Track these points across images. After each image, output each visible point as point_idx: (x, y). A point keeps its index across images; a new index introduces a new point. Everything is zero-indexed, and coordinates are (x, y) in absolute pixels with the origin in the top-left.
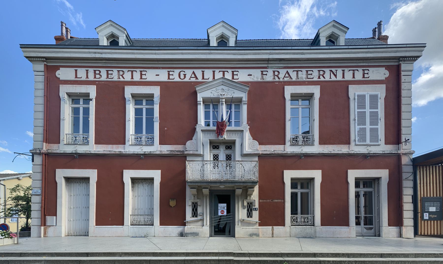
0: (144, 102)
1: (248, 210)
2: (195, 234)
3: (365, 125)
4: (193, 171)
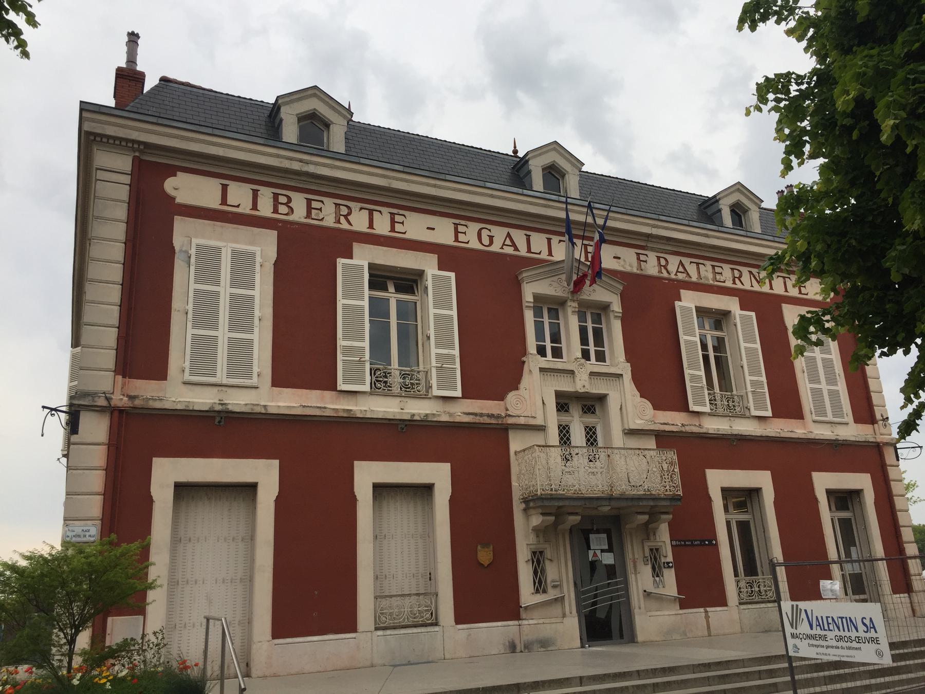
0: (391, 289)
1: (654, 568)
2: (545, 643)
3: (216, 328)
4: (540, 466)
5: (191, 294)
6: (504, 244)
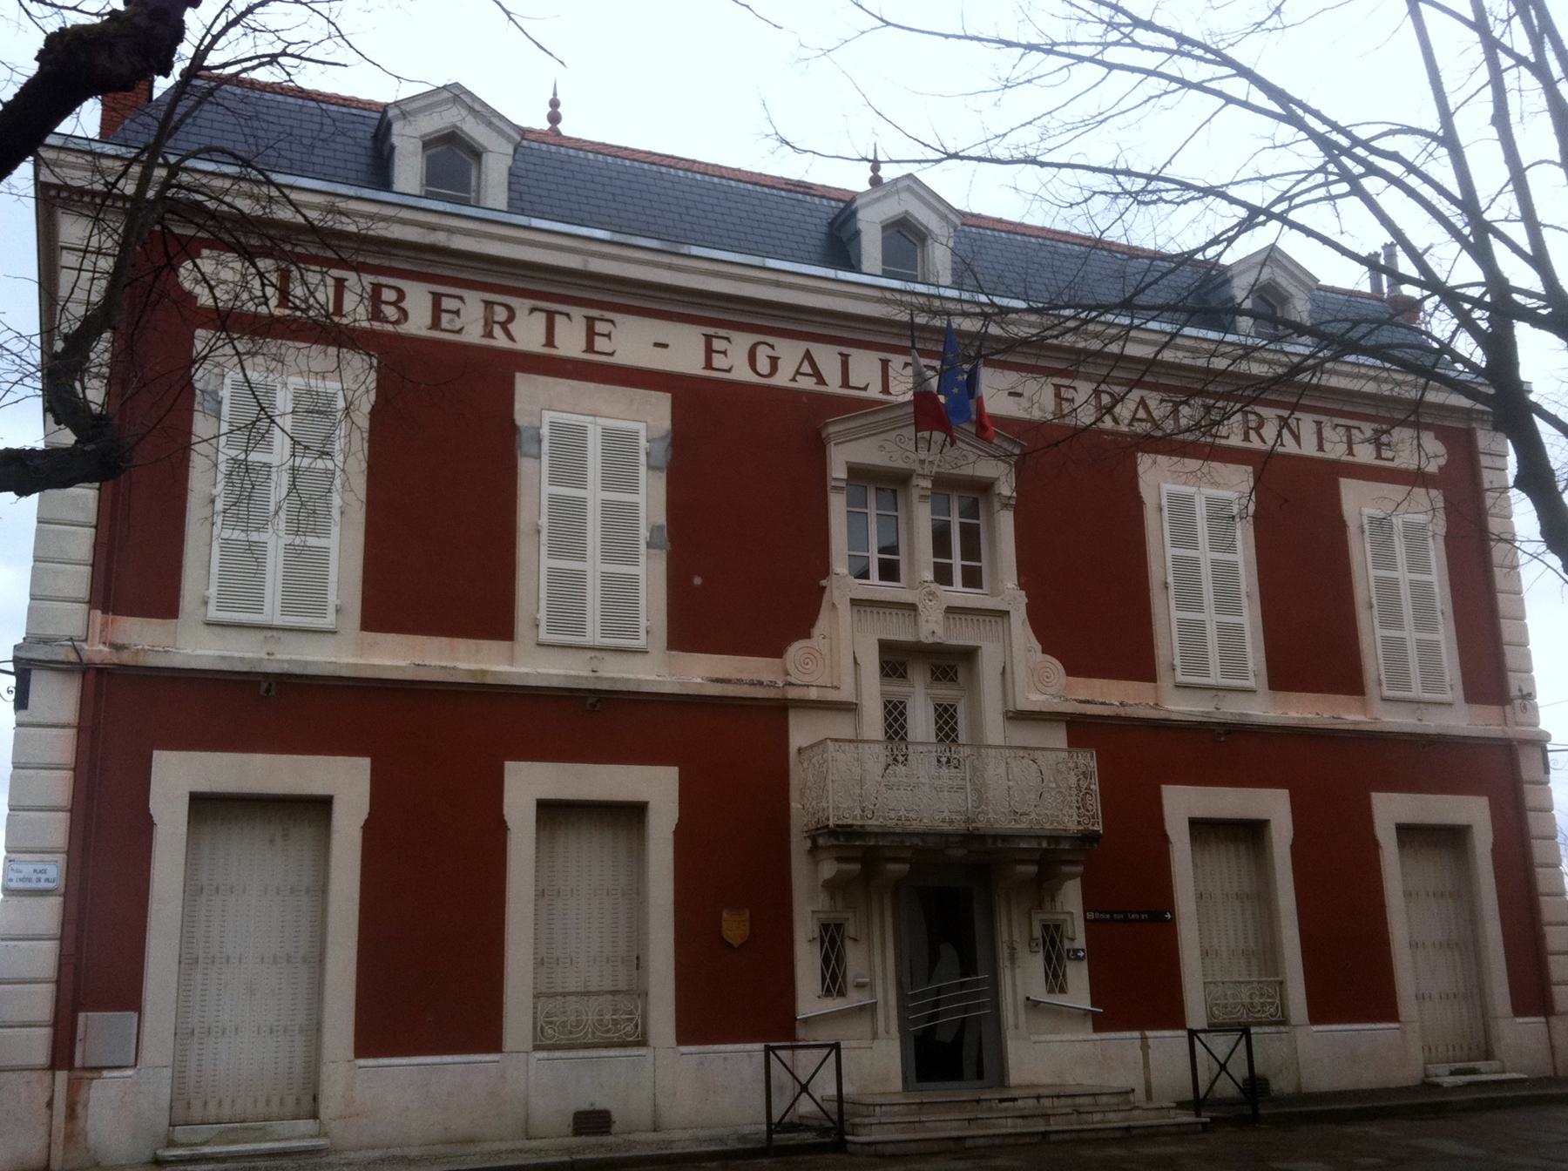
1: (1048, 959)
5: (1169, 563)
6: (798, 372)
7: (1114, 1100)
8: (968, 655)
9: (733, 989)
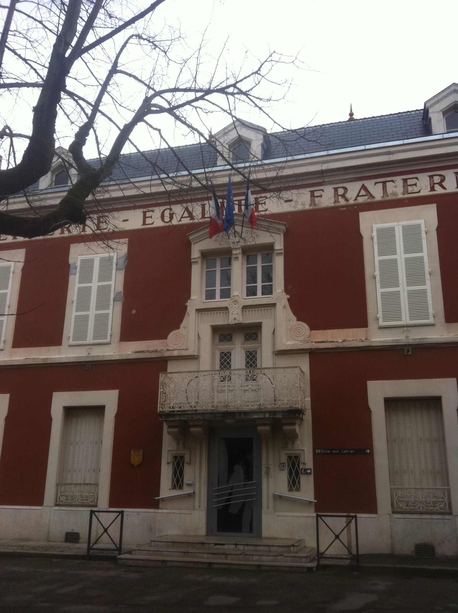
1: (290, 473)
5: (377, 264)
7: (281, 550)
8: (258, 327)
9: (134, 485)
